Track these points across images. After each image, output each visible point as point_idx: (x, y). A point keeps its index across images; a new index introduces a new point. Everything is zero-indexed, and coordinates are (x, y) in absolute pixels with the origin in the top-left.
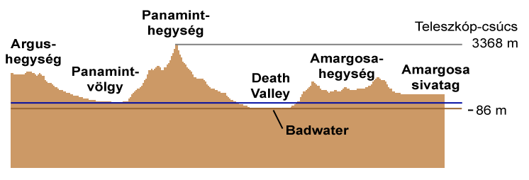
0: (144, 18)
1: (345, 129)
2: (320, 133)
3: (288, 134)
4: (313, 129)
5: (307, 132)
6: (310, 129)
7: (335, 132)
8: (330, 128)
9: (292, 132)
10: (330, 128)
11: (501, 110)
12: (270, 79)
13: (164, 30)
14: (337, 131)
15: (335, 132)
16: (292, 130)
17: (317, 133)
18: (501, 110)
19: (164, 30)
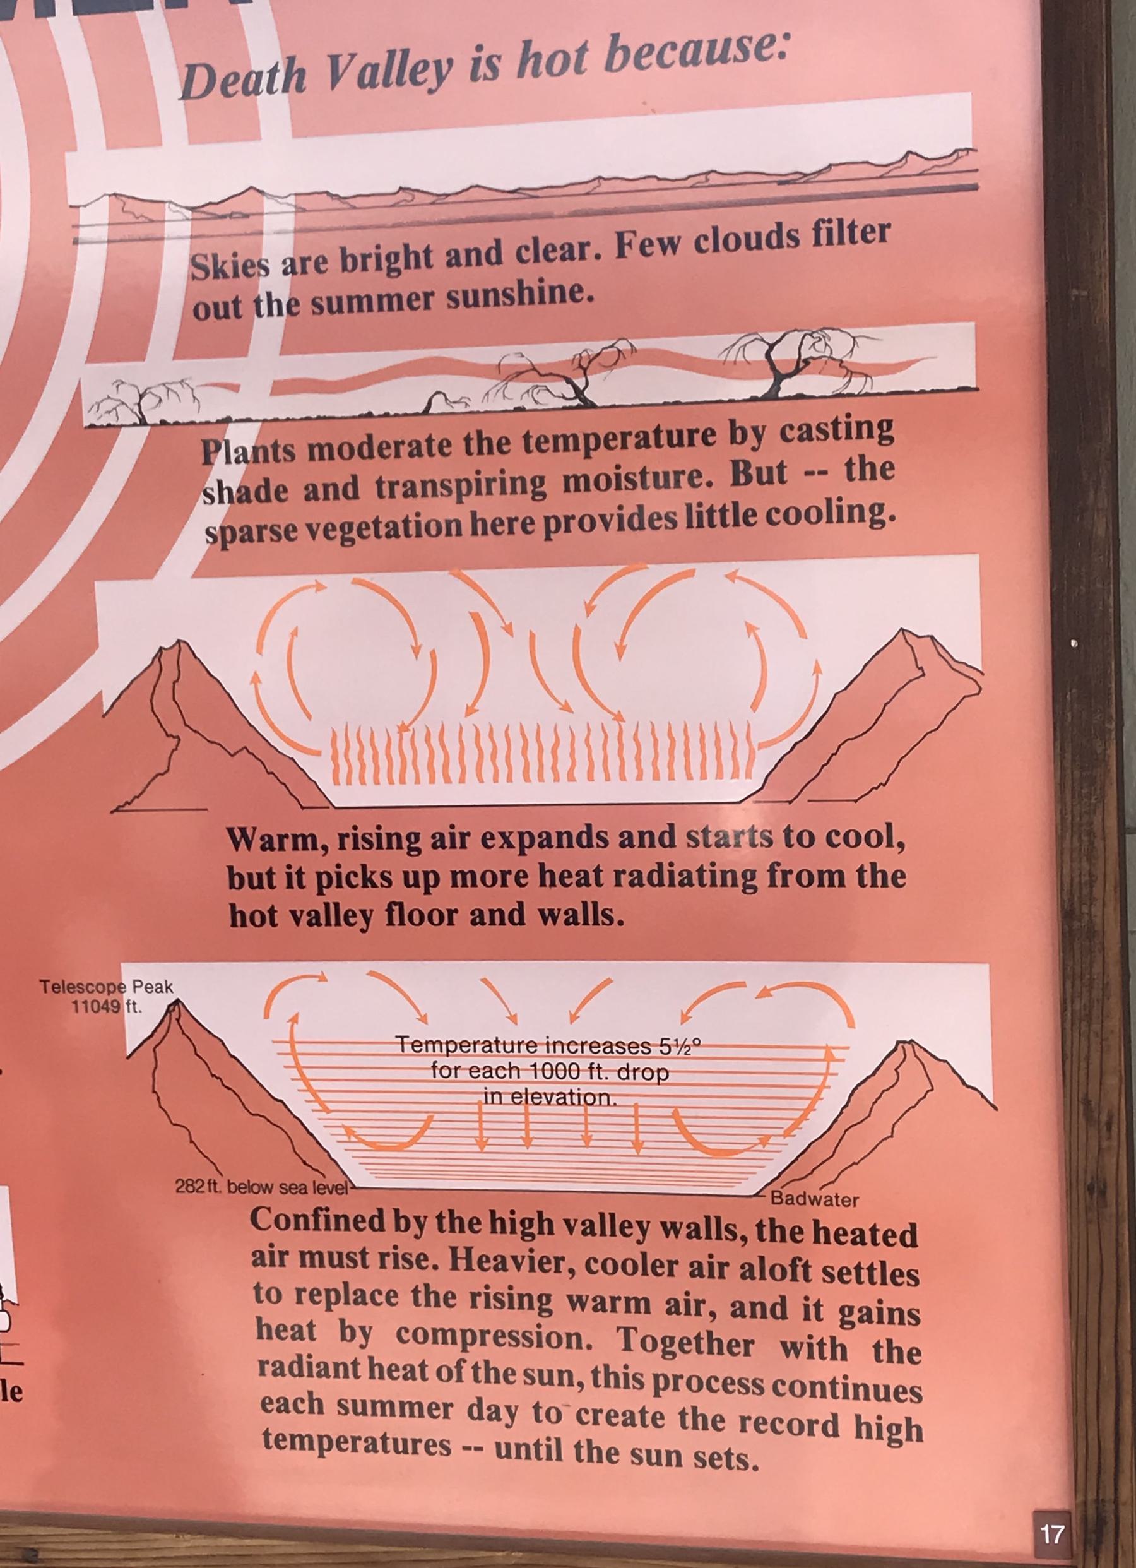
0: (135, 991)
1: (855, 1199)
2: (818, 1204)
3: (773, 1203)
4: (809, 1197)
5: (801, 1200)
6: (804, 1196)
7: (648, 1420)
8: (492, 1040)
9: (535, 1096)
10: (492, 1040)
11: (824, 473)
12: (155, 987)
13: (898, 1234)
14: (843, 1201)
15: (648, 1420)
16: (780, 1197)
17: (267, 1192)
18: (824, 473)
19: (898, 1234)
